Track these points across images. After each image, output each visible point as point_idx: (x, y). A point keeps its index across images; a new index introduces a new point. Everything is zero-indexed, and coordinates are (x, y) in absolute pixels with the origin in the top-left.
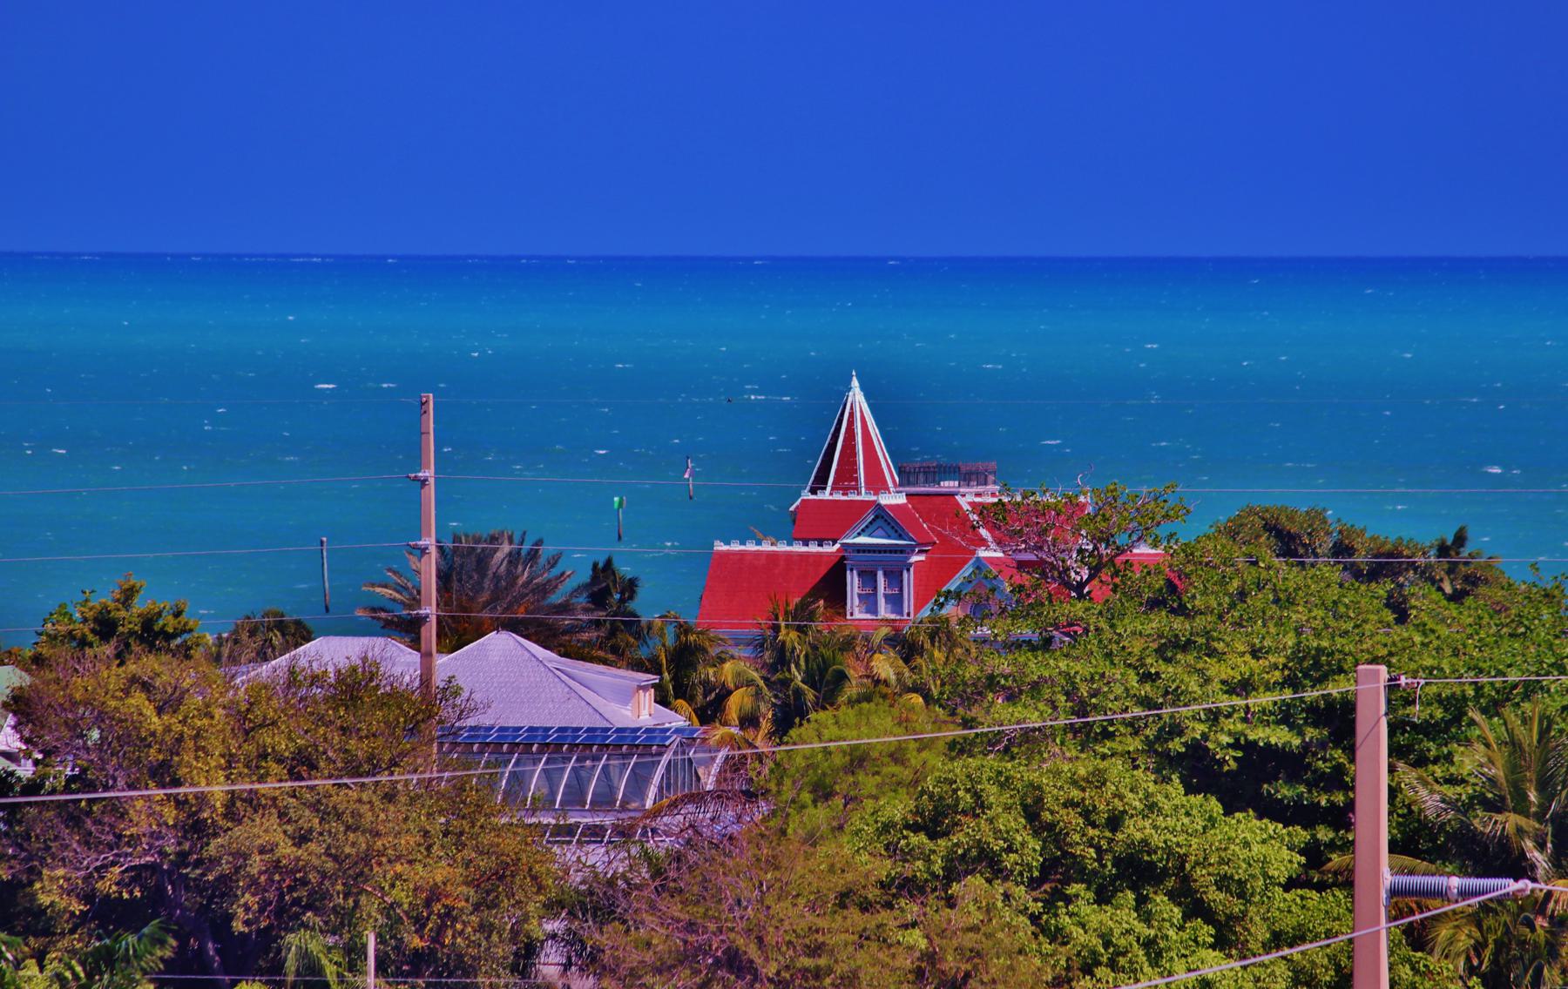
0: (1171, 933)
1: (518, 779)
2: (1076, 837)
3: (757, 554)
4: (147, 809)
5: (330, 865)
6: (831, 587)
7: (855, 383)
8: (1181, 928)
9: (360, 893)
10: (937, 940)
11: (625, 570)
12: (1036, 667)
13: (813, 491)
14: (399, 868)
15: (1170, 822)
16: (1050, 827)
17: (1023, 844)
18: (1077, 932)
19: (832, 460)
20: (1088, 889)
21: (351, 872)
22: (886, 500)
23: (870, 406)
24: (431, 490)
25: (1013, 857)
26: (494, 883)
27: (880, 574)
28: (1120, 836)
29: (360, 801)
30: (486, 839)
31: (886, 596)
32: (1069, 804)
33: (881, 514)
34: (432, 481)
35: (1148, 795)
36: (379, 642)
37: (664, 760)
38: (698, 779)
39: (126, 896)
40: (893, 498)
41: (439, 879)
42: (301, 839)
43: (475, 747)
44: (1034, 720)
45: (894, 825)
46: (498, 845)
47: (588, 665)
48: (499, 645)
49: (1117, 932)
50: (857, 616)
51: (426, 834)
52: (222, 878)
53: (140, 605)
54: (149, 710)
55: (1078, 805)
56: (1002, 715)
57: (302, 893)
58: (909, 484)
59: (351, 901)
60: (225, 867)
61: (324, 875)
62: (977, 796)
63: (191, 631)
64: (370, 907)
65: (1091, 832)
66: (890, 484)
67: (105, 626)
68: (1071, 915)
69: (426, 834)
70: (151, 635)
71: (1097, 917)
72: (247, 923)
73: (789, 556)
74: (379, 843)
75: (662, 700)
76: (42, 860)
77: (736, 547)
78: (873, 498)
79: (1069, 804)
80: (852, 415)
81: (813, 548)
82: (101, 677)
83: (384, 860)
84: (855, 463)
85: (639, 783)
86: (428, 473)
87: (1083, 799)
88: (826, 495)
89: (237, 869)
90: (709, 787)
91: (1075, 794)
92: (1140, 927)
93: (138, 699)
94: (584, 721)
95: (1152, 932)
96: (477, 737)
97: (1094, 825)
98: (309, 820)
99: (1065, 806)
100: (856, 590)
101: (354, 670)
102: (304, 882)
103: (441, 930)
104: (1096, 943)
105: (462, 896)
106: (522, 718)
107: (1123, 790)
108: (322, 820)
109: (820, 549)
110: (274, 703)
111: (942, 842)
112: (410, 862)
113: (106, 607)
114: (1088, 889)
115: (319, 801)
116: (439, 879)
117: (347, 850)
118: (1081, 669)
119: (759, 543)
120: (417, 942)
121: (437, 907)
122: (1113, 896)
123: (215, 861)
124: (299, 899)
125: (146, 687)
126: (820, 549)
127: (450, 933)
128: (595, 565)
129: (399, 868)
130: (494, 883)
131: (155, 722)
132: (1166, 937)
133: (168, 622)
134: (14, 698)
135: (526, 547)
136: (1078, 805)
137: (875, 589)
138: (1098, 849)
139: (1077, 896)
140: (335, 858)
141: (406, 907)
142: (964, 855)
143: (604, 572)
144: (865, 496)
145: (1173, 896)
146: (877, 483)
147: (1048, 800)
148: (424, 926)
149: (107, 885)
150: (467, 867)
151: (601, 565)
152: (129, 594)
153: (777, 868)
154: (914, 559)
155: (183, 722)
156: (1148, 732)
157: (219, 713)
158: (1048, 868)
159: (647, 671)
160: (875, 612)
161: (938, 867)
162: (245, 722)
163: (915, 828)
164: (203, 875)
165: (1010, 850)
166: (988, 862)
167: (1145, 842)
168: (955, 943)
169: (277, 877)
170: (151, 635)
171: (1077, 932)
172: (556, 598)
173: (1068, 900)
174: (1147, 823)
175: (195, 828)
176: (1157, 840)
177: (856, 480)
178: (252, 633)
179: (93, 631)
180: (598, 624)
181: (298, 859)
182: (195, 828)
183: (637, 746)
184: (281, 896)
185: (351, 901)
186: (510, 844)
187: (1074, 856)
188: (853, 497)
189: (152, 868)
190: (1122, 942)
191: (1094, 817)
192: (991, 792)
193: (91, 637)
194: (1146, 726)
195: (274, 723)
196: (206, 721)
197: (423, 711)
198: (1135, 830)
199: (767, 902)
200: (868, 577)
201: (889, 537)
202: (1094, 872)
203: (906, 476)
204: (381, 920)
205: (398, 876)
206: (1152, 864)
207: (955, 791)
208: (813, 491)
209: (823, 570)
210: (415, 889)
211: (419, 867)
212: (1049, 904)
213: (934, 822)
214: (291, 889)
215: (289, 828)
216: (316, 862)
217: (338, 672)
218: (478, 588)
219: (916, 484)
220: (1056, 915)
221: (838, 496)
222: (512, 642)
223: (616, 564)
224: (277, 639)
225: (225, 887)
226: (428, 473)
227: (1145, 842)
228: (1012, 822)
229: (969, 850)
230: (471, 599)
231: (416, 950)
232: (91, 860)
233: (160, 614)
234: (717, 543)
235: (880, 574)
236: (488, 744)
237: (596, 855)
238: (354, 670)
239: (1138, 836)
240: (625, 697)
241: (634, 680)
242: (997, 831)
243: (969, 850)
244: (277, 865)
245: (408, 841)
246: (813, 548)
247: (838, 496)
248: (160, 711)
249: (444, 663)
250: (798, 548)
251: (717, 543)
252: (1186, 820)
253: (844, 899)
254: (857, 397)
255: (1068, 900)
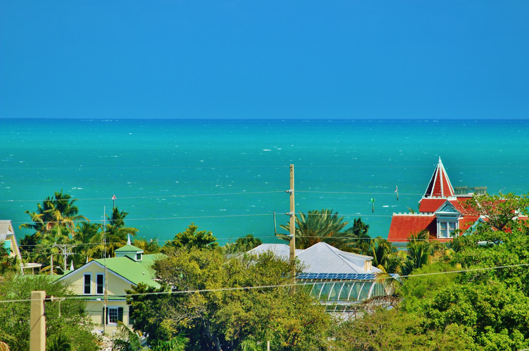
0: (520, 343)
1: (326, 290)
2: (488, 311)
3: (408, 217)
4: (197, 301)
5: (257, 319)
6: (432, 228)
7: (440, 161)
8: (524, 341)
9: (267, 328)
10: (439, 344)
11: (365, 222)
12: (485, 253)
13: (426, 196)
14: (279, 320)
15: (520, 305)
16: (480, 307)
17: (471, 313)
18: (488, 342)
19: (434, 187)
20: (492, 328)
21: (264, 321)
22: (450, 199)
23: (445, 168)
24: (293, 197)
25: (467, 317)
26: (311, 325)
27: (448, 224)
28: (503, 310)
29: (266, 297)
30: (308, 310)
31: (450, 231)
32: (486, 300)
33: (448, 204)
34: (293, 193)
35: (512, 296)
36: (273, 245)
37: (374, 284)
38: (385, 291)
39: (190, 328)
40: (453, 198)
41: (292, 323)
42: (248, 310)
43: (302, 280)
44: (483, 270)
45: (429, 306)
46: (312, 312)
47: (350, 253)
48: (321, 246)
49: (502, 342)
50: (440, 237)
51: (288, 308)
52: (222, 323)
53: (196, 233)
54: (197, 267)
55: (489, 300)
56: (474, 269)
57: (248, 328)
58: (457, 194)
59: (263, 331)
60: (223, 319)
61: (255, 323)
62: (457, 297)
63: (214, 241)
64: (270, 333)
65: (493, 309)
66: (452, 194)
67: (185, 240)
68: (487, 336)
69: (288, 308)
70: (201, 242)
71: (494, 337)
72: (230, 337)
73: (418, 218)
74: (273, 312)
75: (375, 265)
76: (163, 317)
77: (400, 214)
78: (446, 198)
79: (486, 300)
80: (439, 171)
81: (426, 215)
82: (184, 257)
83: (274, 317)
84: (440, 187)
85: (365, 291)
86: (292, 190)
87: (490, 298)
88: (430, 198)
89: (227, 320)
90: (388, 294)
91: (488, 296)
92: (510, 341)
93: (194, 264)
94: (347, 271)
95: (514, 342)
96: (370, 277)
97: (494, 306)
98: (250, 303)
99: (485, 300)
100: (440, 229)
101: (265, 255)
102: (248, 324)
103: (293, 340)
104: (495, 346)
105: (300, 329)
106: (328, 271)
107: (504, 295)
108: (254, 304)
109: (428, 215)
110: (239, 265)
111: (444, 313)
112: (283, 318)
113: (185, 234)
114: (492, 328)
115: (253, 298)
116: (292, 323)
117: (262, 314)
118: (500, 254)
119: (408, 213)
120: (285, 344)
121: (292, 333)
122: (501, 330)
123: (219, 317)
124: (247, 330)
125: (197, 260)
126: (428, 215)
127: (296, 341)
128: (355, 220)
129: (279, 320)
130: (311, 325)
131: (199, 271)
132: (519, 344)
133: (206, 237)
134: (156, 264)
135: (332, 215)
136: (489, 300)
137: (446, 228)
138: (496, 314)
139: (489, 330)
140: (258, 316)
141: (282, 332)
142: (451, 317)
143: (358, 223)
144: (443, 198)
145: (521, 330)
146: (447, 193)
147: (479, 299)
148: (287, 339)
149: (184, 323)
150: (302, 319)
151: (357, 220)
152: (193, 229)
153: (385, 320)
154: (460, 218)
155: (209, 271)
156: (523, 276)
157: (220, 268)
158: (480, 320)
159: (369, 255)
160: (446, 236)
161: (443, 320)
162: (230, 272)
163: (435, 307)
164: (216, 321)
165: (466, 315)
166: (459, 319)
167: (511, 312)
168: (445, 345)
169: (240, 323)
170: (201, 242)
171: (488, 342)
172: (342, 231)
173: (486, 332)
174: (512, 306)
175: (213, 307)
176: (515, 312)
177: (440, 192)
178: (243, 243)
179: (181, 242)
180: (356, 240)
181: (247, 317)
182: (213, 307)
183: (365, 281)
184: (241, 329)
185: (263, 331)
186: (315, 312)
187: (487, 317)
188: (439, 198)
189: (200, 319)
190: (504, 345)
191: (495, 304)
192: (461, 296)
193: (180, 244)
194: (522, 274)
195: (239, 272)
196: (217, 271)
197: (289, 268)
198: (507, 308)
199: (382, 331)
200: (444, 224)
201: (451, 211)
202: (495, 322)
203: (457, 191)
204: (274, 337)
205: (279, 323)
206: (514, 320)
207: (450, 295)
208: (426, 196)
209: (429, 222)
210: (285, 327)
211: (286, 319)
212: (479, 334)
213: (441, 306)
214: (244, 327)
215: (244, 307)
216: (252, 318)
217: (260, 256)
218: (316, 228)
219: (459, 194)
220: (481, 337)
221: (435, 198)
222: (325, 246)
223: (362, 221)
224: (251, 244)
225: (223, 325)
226: (292, 190)
227: (511, 312)
228: (467, 306)
229: (453, 315)
230: (313, 232)
231: (285, 347)
232: (180, 317)
233: (203, 234)
234: (394, 213)
235: (448, 224)
236: (316, 279)
237: (345, 317)
238: (265, 255)
239: (509, 310)
240: (362, 264)
241: (365, 258)
242: (462, 309)
243: (453, 315)
244: (239, 319)
245: (283, 311)
246: (426, 215)
247: (435, 198)
248: (201, 268)
249: (299, 253)
250: (421, 215)
251: (394, 213)
252: (525, 305)
253: (408, 330)
254: (441, 165)
255: (486, 332)
